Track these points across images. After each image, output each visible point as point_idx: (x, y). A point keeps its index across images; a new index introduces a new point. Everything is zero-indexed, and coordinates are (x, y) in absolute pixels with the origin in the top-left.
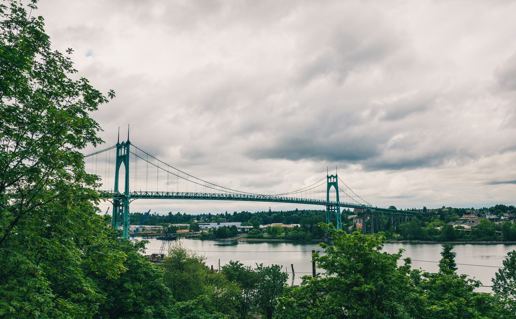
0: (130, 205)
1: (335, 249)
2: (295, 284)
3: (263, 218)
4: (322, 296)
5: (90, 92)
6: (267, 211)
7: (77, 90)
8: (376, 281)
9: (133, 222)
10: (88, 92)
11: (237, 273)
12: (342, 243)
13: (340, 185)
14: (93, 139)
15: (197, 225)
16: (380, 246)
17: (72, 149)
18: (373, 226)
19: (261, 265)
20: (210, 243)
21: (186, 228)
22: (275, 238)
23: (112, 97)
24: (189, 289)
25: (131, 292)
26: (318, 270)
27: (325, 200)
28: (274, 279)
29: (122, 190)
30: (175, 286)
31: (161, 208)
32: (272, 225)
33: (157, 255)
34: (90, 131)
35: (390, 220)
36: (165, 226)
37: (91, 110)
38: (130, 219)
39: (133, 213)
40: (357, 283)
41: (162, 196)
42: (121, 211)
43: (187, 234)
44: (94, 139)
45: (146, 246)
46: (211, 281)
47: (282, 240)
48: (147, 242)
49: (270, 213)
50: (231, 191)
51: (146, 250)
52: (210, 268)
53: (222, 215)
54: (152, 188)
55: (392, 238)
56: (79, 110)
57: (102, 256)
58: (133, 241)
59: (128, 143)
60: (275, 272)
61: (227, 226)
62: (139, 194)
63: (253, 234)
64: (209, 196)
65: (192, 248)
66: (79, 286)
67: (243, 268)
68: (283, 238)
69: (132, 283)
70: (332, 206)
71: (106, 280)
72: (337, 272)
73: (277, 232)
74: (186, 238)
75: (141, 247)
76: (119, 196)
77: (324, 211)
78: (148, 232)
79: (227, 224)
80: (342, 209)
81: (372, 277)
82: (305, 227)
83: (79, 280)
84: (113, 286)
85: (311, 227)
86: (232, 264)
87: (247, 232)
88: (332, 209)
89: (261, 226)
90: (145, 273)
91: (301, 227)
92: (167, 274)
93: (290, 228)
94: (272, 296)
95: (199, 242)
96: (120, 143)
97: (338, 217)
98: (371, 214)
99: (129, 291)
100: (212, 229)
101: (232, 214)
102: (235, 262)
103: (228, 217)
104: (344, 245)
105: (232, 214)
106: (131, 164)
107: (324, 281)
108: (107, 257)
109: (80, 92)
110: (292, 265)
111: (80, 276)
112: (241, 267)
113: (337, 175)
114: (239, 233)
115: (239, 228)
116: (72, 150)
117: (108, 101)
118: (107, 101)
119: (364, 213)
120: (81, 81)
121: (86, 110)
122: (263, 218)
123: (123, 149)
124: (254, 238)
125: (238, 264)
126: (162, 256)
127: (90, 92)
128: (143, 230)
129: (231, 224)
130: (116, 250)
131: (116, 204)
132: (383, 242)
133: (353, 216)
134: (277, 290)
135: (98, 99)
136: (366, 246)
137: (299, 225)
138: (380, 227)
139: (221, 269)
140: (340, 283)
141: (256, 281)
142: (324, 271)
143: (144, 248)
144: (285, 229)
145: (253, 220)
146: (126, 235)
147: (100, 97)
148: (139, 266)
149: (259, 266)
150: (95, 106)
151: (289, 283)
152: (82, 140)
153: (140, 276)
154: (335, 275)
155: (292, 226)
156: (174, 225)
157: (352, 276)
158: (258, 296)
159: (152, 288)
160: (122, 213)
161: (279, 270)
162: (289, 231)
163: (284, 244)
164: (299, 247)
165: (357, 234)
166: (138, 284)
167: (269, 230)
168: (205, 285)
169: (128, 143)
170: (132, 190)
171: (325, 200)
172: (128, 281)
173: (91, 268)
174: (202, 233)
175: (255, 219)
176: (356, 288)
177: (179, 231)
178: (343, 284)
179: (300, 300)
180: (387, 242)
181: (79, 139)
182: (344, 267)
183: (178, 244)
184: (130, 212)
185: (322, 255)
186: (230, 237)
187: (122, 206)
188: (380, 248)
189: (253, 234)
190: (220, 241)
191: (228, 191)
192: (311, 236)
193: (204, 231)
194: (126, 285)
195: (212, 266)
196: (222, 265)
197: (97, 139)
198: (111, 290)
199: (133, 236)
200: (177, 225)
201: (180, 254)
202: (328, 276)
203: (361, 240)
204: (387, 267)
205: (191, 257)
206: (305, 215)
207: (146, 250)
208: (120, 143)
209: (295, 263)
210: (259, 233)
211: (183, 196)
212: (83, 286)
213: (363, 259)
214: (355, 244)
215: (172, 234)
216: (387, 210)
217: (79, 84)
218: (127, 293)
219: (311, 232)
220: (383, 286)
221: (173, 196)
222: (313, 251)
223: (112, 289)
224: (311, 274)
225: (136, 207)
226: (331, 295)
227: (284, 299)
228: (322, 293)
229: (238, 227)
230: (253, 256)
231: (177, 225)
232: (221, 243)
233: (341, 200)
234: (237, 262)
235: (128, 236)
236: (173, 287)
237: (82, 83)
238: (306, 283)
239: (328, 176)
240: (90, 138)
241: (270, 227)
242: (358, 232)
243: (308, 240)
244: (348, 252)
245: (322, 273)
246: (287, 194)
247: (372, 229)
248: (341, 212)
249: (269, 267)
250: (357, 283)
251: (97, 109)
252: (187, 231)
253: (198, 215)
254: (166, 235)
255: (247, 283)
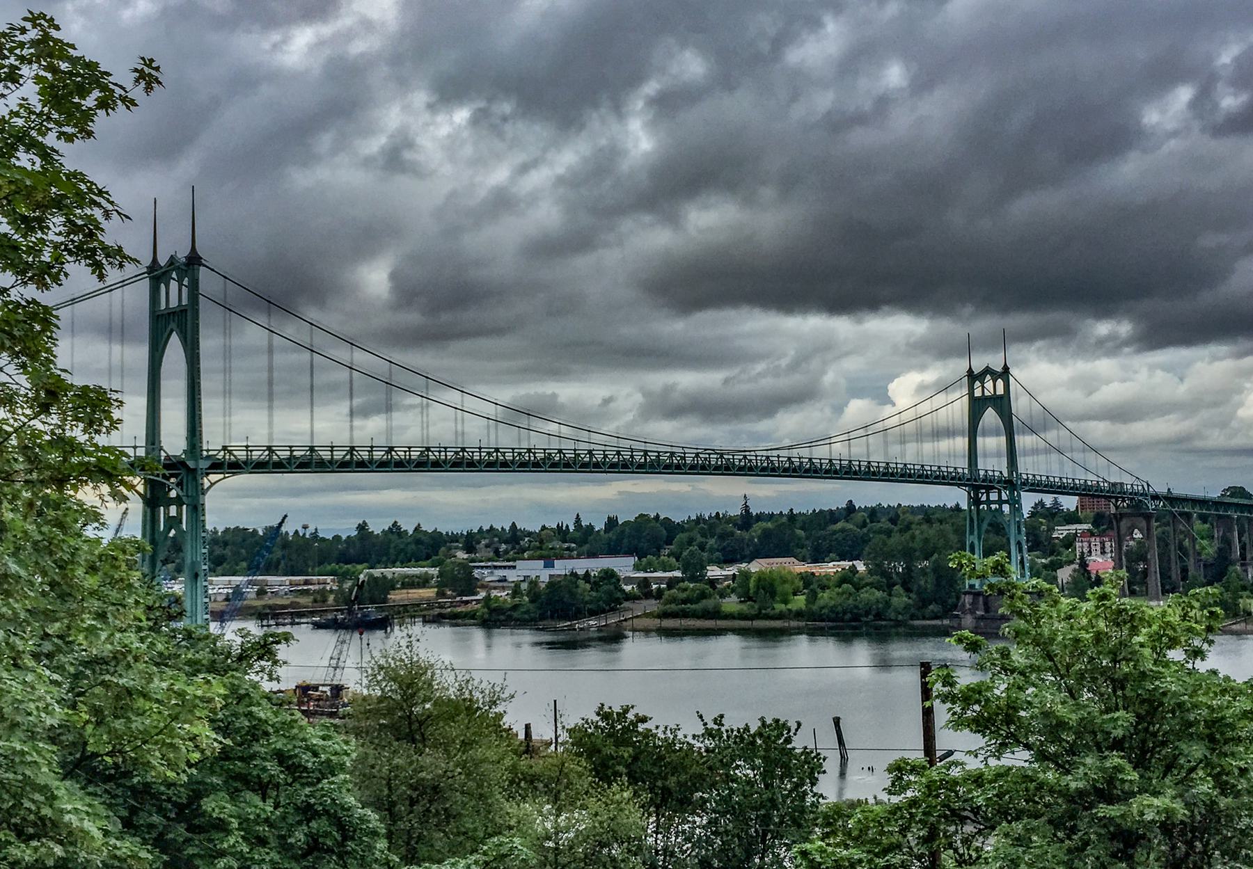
0: (209, 501)
1: (1018, 657)
2: (851, 795)
3: (722, 537)
4: (966, 841)
5: (64, 66)
6: (736, 511)
7: (12, 60)
8: (1185, 782)
9: (219, 564)
10: (53, 69)
11: (626, 752)
12: (1046, 632)
13: (1020, 405)
14: (89, 247)
15: (466, 569)
16: (1197, 642)
17: (13, 292)
18: (1155, 566)
19: (719, 720)
20: (516, 639)
21: (423, 582)
22: (768, 617)
23: (149, 88)
24: (449, 816)
25: (228, 832)
26: (946, 739)
27: (962, 464)
28: (767, 775)
29: (174, 442)
30: (393, 804)
31: (327, 509)
32: (755, 567)
33: (316, 688)
34: (80, 222)
35: (1227, 542)
36: (343, 577)
37: (69, 138)
38: (211, 552)
39: (221, 530)
40: (1108, 791)
41: (331, 462)
42: (173, 522)
43: (430, 605)
44: (94, 251)
45: (282, 651)
46: (526, 784)
47: (794, 624)
48: (287, 638)
49: (747, 520)
50: (595, 438)
51: (281, 671)
52: (522, 736)
53: (561, 532)
54: (295, 427)
55: (1236, 615)
56: (23, 139)
57: (129, 692)
58: (232, 634)
59: (194, 260)
60: (772, 747)
61: (581, 572)
62: (241, 455)
63: (684, 602)
64: (509, 456)
65: (455, 658)
66: (46, 811)
67: (648, 734)
68: (799, 615)
69: (234, 795)
70: (989, 489)
71: (133, 788)
72: (1028, 747)
73: (773, 594)
74: (426, 621)
75: (260, 658)
76: (166, 467)
77: (957, 508)
78: (279, 602)
79: (581, 566)
80: (1028, 501)
81: (1168, 769)
82: (894, 572)
83: (44, 789)
84: (161, 811)
85: (908, 569)
86: (606, 716)
87: (659, 594)
88: (988, 502)
89: (714, 572)
90: (281, 757)
91: (870, 572)
92: (362, 759)
93: (827, 576)
94: (763, 841)
95: (478, 635)
96: (163, 260)
97: (1013, 531)
98: (1148, 517)
99: (221, 826)
100: (524, 586)
101: (599, 526)
102: (617, 709)
103: (581, 539)
104: (1052, 640)
105: (599, 526)
106: (209, 343)
107: (978, 780)
108: (145, 696)
109: (25, 70)
110: (837, 721)
111: (46, 775)
112: (641, 727)
113: (1006, 369)
114: (630, 597)
115: (629, 580)
116: (14, 295)
117: (133, 102)
118: (130, 103)
119: (1119, 517)
120: (28, 25)
121: (50, 140)
122: (722, 537)
123: (174, 285)
124: (685, 615)
125: (630, 716)
126: (337, 690)
127: (64, 66)
128: (261, 593)
129: (596, 565)
130: (170, 672)
131: (154, 499)
132: (1209, 629)
133: (1073, 528)
134: (782, 817)
135: (96, 94)
136: (1142, 645)
137: (861, 567)
138: (1185, 571)
139: (564, 736)
140: (1040, 786)
141: (699, 782)
142: (977, 741)
143: (275, 662)
144: (807, 579)
145: (681, 547)
146: (194, 614)
147: (104, 88)
148: (257, 731)
149: (711, 725)
150: (81, 124)
151: (828, 790)
152: (46, 257)
153: (264, 769)
154: (1018, 758)
155: (831, 568)
156: (377, 572)
157: (1089, 761)
158: (709, 842)
159: (308, 812)
160: (180, 531)
161: (788, 740)
162: (823, 588)
163: (804, 637)
164: (862, 652)
165: (1104, 597)
166: (257, 800)
167: (742, 584)
168: (510, 797)
169: (194, 260)
170: (212, 441)
171: (962, 464)
172: (215, 789)
173: (85, 744)
174: (488, 599)
175: (690, 542)
176: (1104, 810)
177: (397, 596)
178: (1051, 791)
179: (885, 852)
180: (1225, 632)
181: (35, 250)
182: (1055, 727)
183: (404, 643)
184: (209, 527)
185: (966, 678)
186: (593, 614)
187: (178, 502)
188: (1197, 653)
189: (684, 602)
190: (556, 631)
191: (584, 436)
192: (907, 607)
193: (494, 593)
194: (209, 805)
195: (528, 727)
196: (572, 720)
197: (105, 248)
198: (151, 826)
199: (220, 617)
200: (389, 572)
201: (411, 681)
202: (993, 762)
203: (1120, 618)
204: (1232, 727)
205: (452, 693)
206: (884, 524)
207: (281, 671)
208: (163, 260)
209: (861, 715)
210: (703, 596)
211: (410, 461)
212: (62, 811)
213: (1128, 693)
214: (1099, 638)
215: (371, 608)
216: (1217, 504)
217: (21, 38)
218: (216, 835)
219: (908, 590)
220: (1213, 803)
221: (371, 461)
222: (926, 668)
223: (156, 819)
224: (917, 755)
225: (231, 505)
226: (1007, 835)
227: (822, 851)
228: (969, 829)
229: (622, 575)
230: (680, 686)
231: (389, 572)
232: (561, 637)
233: (1028, 467)
234: (626, 710)
235: (201, 617)
236: (387, 808)
237: (33, 34)
238: (904, 789)
239: (970, 371)
240: (80, 248)
241: (746, 575)
242: (1107, 588)
243: (898, 624)
244: (1068, 667)
245: (966, 749)
246: (811, 444)
247: (1155, 580)
248: (1026, 509)
249: (747, 729)
250: (1108, 791)
251: (90, 134)
252: (429, 593)
253: (470, 534)
254: (350, 612)
255: (666, 791)
